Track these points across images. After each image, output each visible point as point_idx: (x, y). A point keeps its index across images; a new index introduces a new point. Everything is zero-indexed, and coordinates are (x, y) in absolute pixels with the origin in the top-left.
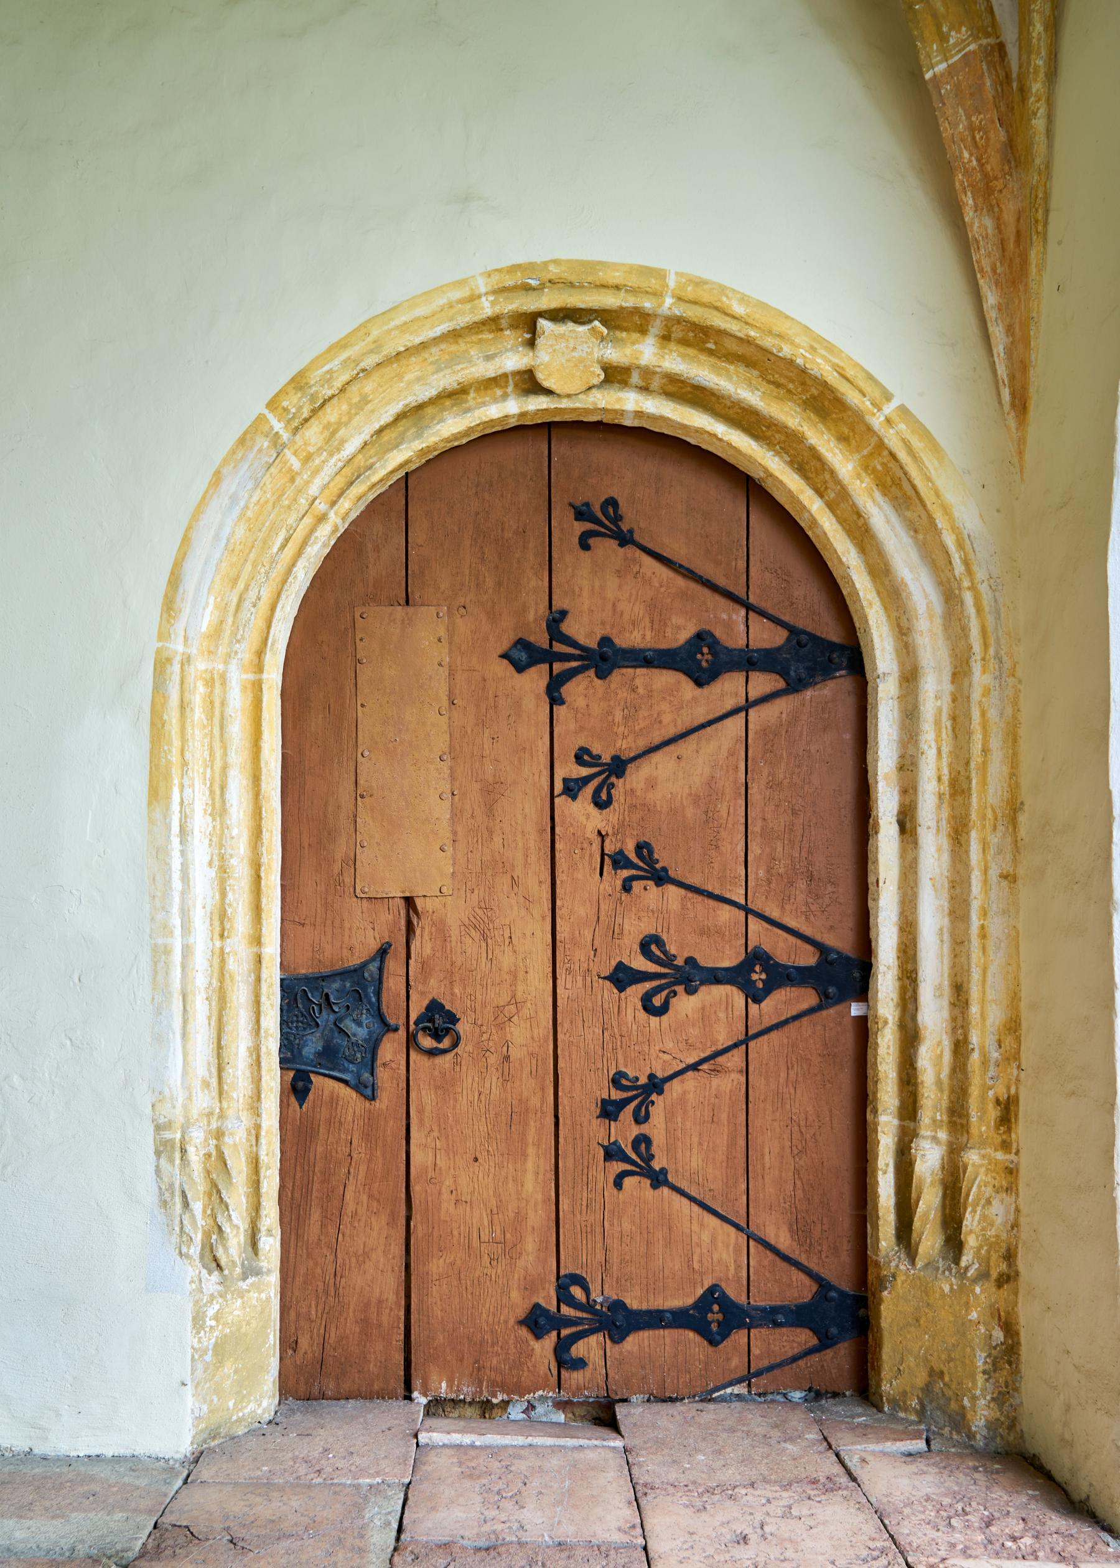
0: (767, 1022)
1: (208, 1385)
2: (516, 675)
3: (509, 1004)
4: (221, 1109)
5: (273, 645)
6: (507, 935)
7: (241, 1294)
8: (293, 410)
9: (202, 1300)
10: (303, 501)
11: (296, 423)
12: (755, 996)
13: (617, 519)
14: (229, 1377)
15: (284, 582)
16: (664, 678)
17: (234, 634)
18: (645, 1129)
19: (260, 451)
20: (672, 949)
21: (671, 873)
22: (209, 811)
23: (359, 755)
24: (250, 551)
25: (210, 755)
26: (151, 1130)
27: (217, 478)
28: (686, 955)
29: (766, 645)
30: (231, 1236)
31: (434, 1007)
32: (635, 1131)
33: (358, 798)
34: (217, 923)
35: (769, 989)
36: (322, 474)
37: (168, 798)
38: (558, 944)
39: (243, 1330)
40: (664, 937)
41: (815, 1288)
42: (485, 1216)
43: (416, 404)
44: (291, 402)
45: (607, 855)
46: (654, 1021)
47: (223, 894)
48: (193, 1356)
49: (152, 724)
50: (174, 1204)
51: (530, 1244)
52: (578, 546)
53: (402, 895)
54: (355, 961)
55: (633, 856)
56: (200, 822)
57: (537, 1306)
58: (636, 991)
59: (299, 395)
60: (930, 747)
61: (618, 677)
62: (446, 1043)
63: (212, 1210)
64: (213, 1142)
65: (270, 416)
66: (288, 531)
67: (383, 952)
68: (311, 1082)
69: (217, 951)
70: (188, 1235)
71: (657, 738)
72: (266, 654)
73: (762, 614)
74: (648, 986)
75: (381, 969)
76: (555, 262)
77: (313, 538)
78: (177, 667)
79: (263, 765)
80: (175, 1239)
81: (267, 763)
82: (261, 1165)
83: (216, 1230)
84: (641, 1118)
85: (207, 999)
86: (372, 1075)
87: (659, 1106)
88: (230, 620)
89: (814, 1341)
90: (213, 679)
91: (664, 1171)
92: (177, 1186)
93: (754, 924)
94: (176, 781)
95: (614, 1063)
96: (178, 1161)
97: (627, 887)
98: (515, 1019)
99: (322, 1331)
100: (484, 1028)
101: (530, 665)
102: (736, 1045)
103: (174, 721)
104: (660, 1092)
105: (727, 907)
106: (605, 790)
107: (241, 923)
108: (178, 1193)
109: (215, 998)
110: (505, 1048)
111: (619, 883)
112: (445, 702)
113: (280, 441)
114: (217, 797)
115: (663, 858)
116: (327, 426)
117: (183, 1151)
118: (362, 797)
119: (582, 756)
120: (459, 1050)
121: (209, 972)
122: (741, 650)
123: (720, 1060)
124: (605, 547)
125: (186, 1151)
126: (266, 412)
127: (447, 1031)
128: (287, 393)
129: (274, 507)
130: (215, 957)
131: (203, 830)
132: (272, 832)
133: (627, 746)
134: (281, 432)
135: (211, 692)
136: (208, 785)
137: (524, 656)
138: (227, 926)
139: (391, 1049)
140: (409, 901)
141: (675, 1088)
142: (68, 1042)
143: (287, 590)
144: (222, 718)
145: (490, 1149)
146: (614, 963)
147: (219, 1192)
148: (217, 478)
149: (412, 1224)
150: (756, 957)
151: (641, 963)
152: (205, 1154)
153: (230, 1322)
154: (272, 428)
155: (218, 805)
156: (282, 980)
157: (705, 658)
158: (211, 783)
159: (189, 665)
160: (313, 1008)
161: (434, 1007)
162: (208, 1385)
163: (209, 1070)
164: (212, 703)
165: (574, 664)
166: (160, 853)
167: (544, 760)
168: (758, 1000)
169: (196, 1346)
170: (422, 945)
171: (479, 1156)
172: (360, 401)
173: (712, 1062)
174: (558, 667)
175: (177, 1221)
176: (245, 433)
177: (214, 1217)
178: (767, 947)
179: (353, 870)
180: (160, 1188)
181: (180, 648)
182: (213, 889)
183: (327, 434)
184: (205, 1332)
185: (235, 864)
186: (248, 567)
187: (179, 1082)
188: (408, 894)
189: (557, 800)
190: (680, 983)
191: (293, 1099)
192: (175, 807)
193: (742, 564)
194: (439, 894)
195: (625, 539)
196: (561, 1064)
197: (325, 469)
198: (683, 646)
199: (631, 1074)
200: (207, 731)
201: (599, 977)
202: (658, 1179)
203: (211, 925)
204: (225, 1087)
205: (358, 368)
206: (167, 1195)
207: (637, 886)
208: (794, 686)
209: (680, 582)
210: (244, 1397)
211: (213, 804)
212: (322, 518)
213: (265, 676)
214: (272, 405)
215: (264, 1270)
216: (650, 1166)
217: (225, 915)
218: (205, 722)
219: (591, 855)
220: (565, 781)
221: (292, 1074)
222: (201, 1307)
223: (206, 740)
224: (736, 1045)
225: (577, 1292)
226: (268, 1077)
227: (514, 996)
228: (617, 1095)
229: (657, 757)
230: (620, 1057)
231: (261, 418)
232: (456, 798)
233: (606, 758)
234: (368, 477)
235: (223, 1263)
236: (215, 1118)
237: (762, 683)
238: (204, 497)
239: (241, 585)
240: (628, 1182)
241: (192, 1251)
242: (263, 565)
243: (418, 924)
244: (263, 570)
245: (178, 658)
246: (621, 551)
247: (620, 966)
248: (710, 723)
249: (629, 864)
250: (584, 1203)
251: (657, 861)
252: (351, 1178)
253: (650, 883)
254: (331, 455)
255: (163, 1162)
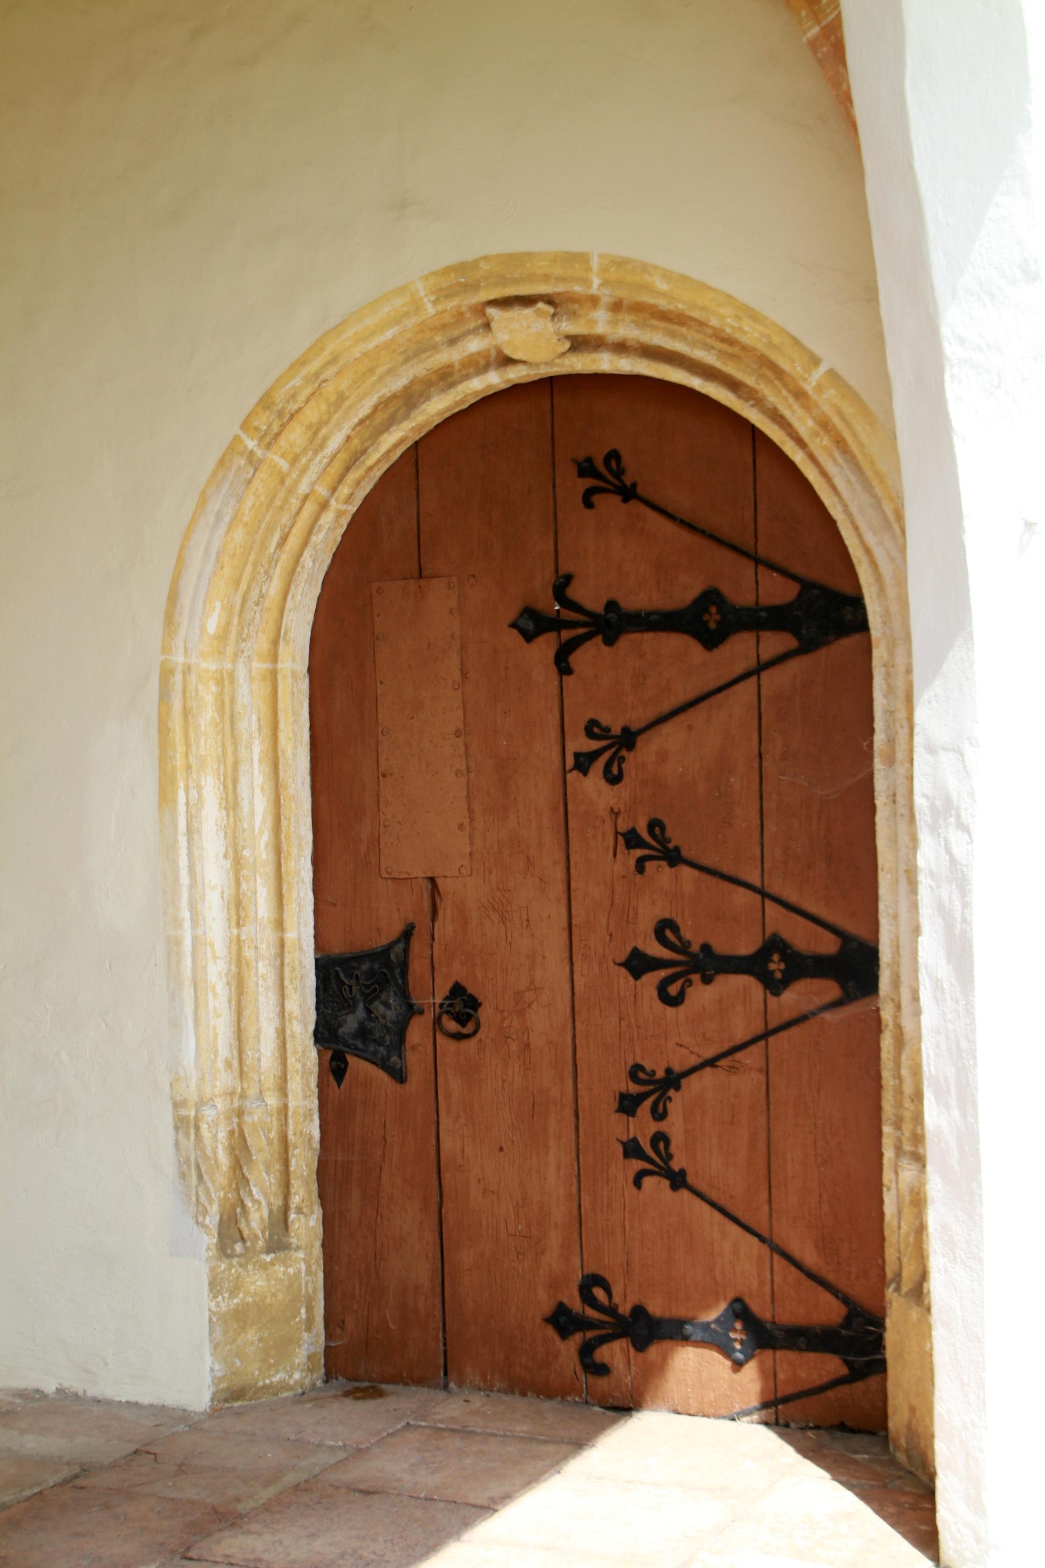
0: (787, 1016)
1: (228, 1347)
2: (525, 644)
3: (528, 989)
4: (242, 1089)
5: (286, 634)
6: (524, 918)
7: (264, 1267)
8: (265, 428)
9: (220, 1267)
10: (293, 501)
11: (267, 439)
12: (774, 986)
13: (619, 473)
14: (252, 1343)
15: (293, 571)
16: (674, 642)
17: (240, 633)
18: (663, 1126)
19: (239, 469)
20: (687, 934)
21: (685, 853)
22: (224, 805)
23: (380, 734)
24: (249, 554)
25: (223, 751)
26: (170, 1107)
27: (203, 500)
28: (701, 942)
29: (777, 601)
30: (252, 1210)
31: (458, 991)
32: (653, 1127)
33: (381, 778)
34: (233, 912)
35: (786, 982)
36: (309, 473)
37: (174, 801)
38: (574, 928)
39: (268, 1301)
40: (679, 921)
41: (843, 1311)
42: (511, 1208)
43: (390, 394)
44: (262, 422)
45: (620, 833)
46: (670, 1011)
47: (238, 884)
48: (210, 1319)
49: (160, 732)
50: (191, 1176)
51: (554, 1241)
52: (582, 505)
53: (423, 875)
54: (383, 941)
55: (645, 835)
56: (212, 814)
57: (561, 1305)
58: (652, 979)
59: (267, 414)
60: (902, 726)
61: (627, 641)
62: (469, 1028)
63: (237, 1184)
64: (235, 1120)
65: (244, 437)
66: (283, 531)
67: (407, 934)
68: (346, 1063)
69: (234, 939)
70: (203, 1205)
71: (666, 707)
72: (279, 644)
73: (772, 566)
74: (663, 973)
75: (406, 951)
76: (486, 258)
77: (317, 527)
78: (178, 677)
79: (280, 755)
80: (192, 1209)
81: (283, 752)
82: (289, 1144)
83: (240, 1204)
84: (659, 1114)
85: (227, 984)
86: (400, 1057)
87: (677, 1103)
88: (235, 621)
89: (844, 1371)
90: (222, 678)
91: (682, 1173)
92: (193, 1157)
93: (771, 907)
94: (181, 784)
95: (631, 1055)
96: (193, 1137)
97: (640, 866)
98: (534, 1006)
99: (366, 1312)
100: (505, 1014)
101: (538, 633)
102: (754, 1041)
103: (178, 728)
104: (678, 1088)
105: (741, 890)
106: (616, 764)
107: (263, 906)
108: (193, 1167)
109: (234, 983)
110: (526, 1035)
111: (632, 863)
112: (457, 675)
113: (254, 458)
114: (230, 791)
115: (676, 836)
116: (309, 427)
117: (197, 1128)
118: (384, 775)
119: (593, 728)
120: (479, 1035)
121: (228, 959)
122: (749, 609)
123: (739, 1056)
124: (609, 504)
125: (199, 1127)
126: (240, 433)
127: (469, 1017)
128: (257, 414)
129: (267, 510)
130: (233, 944)
131: (219, 823)
132: (290, 819)
133: (637, 717)
134: (255, 449)
135: (222, 691)
136: (222, 780)
137: (530, 626)
138: (242, 914)
139: (417, 1032)
140: (432, 880)
141: (693, 1085)
142: (104, 1025)
143: (296, 580)
144: (232, 715)
145: (514, 1139)
146: (629, 949)
147: (241, 1168)
148: (203, 500)
149: (443, 1211)
150: (774, 945)
151: (657, 950)
152: (229, 1131)
153: (252, 1291)
154: (246, 447)
155: (230, 798)
156: (317, 960)
157: (712, 618)
158: (224, 779)
159: (190, 674)
160: (345, 989)
161: (458, 991)
162: (228, 1347)
163: (231, 1052)
164: (223, 701)
165: (581, 631)
166: (169, 849)
167: (553, 733)
168: (776, 994)
169: (214, 1308)
170: (446, 927)
171: (503, 1145)
172: (337, 400)
173: (730, 1058)
174: (566, 635)
175: (193, 1193)
176: (224, 455)
177: (237, 1190)
178: (786, 935)
179: (378, 850)
180: (179, 1161)
181: (181, 659)
182: (229, 879)
183: (310, 433)
184: (224, 1298)
185: (248, 855)
186: (249, 568)
187: (192, 1064)
188: (430, 875)
189: (569, 776)
190: (694, 972)
191: (332, 1078)
192: (182, 808)
193: (749, 514)
194: (458, 875)
195: (629, 494)
196: (579, 1054)
197: (312, 467)
198: (689, 607)
199: (648, 1067)
200: (219, 728)
201: (615, 964)
202: (678, 1181)
203: (229, 913)
204: (245, 1068)
205: (319, 381)
206: (185, 1167)
207: (650, 866)
208: (807, 647)
209: (686, 537)
210: (270, 1366)
211: (227, 799)
212: (324, 506)
213: (280, 666)
214: (245, 426)
215: (294, 1246)
216: (669, 1167)
217: (240, 904)
218: (218, 720)
219: (604, 834)
220: (577, 755)
221: (330, 1054)
222: (218, 1273)
223: (219, 737)
224: (754, 1041)
225: (599, 1293)
226: (293, 1059)
227: (532, 982)
228: (634, 1089)
229: (667, 728)
230: (637, 1048)
231: (237, 439)
232: (472, 775)
233: (616, 730)
234: (363, 462)
235: (245, 1235)
236: (237, 1098)
237: (775, 643)
238: (193, 519)
239: (243, 586)
240: (648, 1182)
241: (207, 1221)
242: (262, 565)
243: (440, 905)
244: (262, 571)
245: (180, 669)
246: (625, 507)
247: (636, 953)
248: (720, 689)
249: (641, 844)
250: (605, 1201)
251: (670, 841)
252: (386, 1161)
253: (664, 863)
254: (316, 453)
255: (181, 1136)
